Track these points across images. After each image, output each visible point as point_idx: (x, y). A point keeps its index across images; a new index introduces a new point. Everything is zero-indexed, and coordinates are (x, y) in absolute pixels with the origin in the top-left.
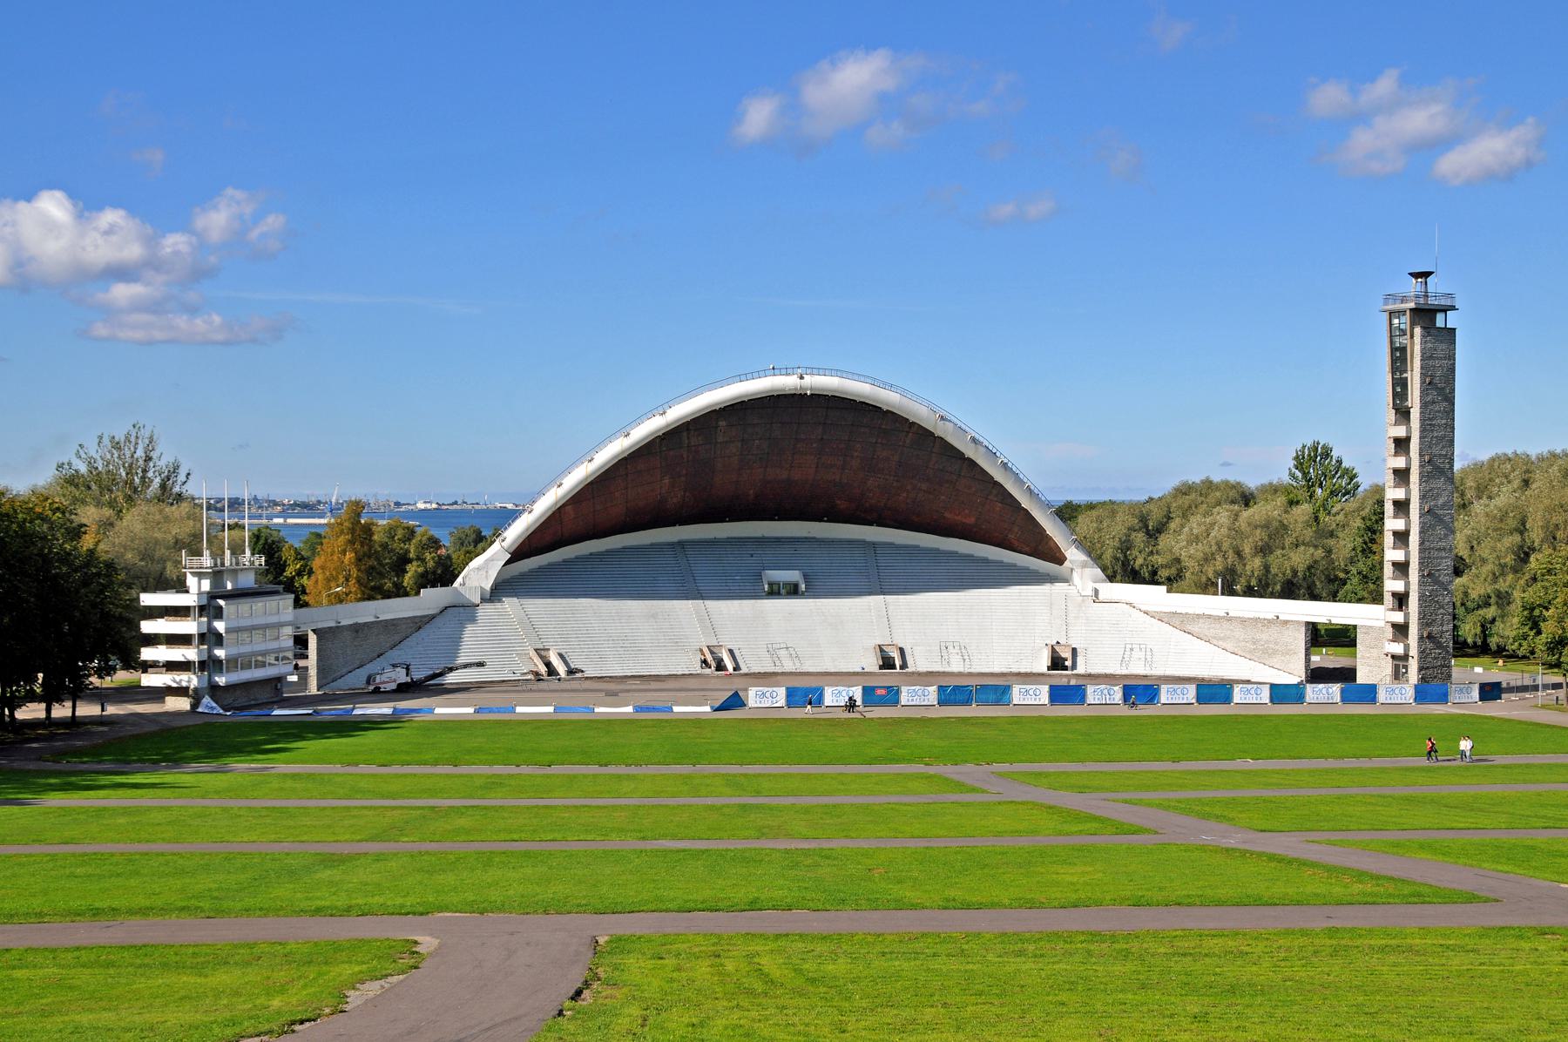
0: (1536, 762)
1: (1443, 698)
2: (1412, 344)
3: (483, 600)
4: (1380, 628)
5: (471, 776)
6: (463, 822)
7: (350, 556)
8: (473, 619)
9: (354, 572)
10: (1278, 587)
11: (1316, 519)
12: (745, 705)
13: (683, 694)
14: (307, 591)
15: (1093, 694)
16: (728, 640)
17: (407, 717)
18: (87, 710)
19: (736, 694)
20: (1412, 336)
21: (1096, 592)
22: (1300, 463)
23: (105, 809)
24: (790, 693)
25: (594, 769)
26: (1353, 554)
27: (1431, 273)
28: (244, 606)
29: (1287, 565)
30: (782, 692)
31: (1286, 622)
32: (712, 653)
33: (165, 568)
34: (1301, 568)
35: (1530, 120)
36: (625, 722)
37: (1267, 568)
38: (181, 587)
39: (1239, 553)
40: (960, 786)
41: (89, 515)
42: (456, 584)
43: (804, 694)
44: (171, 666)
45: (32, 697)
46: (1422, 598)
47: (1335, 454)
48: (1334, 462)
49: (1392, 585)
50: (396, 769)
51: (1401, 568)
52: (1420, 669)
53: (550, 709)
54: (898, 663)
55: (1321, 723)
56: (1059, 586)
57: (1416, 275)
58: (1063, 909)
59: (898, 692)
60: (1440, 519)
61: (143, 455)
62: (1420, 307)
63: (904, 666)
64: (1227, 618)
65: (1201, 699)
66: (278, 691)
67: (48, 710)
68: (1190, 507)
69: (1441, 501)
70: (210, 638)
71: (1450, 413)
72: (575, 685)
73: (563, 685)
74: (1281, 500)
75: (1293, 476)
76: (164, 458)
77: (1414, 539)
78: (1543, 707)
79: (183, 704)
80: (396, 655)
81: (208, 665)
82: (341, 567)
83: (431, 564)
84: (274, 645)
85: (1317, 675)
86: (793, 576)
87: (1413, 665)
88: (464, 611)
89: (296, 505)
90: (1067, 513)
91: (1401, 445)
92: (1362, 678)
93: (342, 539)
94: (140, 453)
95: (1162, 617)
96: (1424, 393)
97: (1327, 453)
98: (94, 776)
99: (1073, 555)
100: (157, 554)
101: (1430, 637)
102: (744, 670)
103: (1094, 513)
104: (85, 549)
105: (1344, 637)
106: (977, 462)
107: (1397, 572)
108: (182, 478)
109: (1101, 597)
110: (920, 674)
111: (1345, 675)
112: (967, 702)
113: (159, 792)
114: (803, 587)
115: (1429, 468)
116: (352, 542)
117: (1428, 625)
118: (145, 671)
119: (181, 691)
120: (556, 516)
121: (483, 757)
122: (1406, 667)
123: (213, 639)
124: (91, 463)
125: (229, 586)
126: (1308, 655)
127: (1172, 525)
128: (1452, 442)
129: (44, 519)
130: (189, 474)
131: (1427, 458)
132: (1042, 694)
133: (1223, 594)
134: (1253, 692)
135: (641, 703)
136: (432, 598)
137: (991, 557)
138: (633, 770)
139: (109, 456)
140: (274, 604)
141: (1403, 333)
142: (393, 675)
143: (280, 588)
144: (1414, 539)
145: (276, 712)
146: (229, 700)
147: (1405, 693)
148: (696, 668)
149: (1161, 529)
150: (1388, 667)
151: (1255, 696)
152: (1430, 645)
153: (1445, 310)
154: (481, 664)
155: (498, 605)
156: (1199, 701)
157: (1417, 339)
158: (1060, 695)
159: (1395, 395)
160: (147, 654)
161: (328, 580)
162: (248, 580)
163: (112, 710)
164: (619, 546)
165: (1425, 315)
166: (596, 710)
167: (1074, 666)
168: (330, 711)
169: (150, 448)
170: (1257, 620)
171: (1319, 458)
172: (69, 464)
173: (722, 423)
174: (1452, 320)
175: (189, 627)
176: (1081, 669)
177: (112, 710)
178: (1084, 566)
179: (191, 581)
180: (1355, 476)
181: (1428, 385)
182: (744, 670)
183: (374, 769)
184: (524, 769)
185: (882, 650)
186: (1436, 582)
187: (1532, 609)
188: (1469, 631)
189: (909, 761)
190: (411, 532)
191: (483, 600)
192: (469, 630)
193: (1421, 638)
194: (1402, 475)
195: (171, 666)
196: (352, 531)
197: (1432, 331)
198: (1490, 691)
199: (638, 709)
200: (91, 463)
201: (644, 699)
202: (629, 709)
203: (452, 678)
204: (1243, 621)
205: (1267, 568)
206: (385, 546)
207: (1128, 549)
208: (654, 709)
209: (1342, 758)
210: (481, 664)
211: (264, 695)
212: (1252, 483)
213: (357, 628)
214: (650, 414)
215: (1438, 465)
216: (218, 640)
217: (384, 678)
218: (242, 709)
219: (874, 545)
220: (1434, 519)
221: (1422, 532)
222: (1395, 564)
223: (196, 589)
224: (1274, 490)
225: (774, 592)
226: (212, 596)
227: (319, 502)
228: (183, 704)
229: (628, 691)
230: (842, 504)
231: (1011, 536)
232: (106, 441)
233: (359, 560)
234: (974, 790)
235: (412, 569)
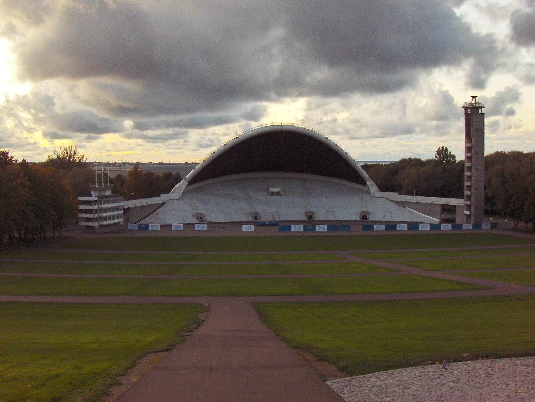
4: (463, 206)
15: (376, 227)
22: (439, 152)
48: (448, 153)
49: (467, 193)
61: (74, 152)
62: (473, 106)
65: (386, 228)
75: (436, 157)
94: (72, 152)
99: (370, 183)
105: (451, 209)
126: (441, 215)
130: (87, 158)
134: (446, 226)
139: (63, 153)
151: (202, 228)
153: (481, 108)
169: (76, 150)
171: (444, 151)
180: (455, 157)
213: (141, 207)
222: (467, 186)
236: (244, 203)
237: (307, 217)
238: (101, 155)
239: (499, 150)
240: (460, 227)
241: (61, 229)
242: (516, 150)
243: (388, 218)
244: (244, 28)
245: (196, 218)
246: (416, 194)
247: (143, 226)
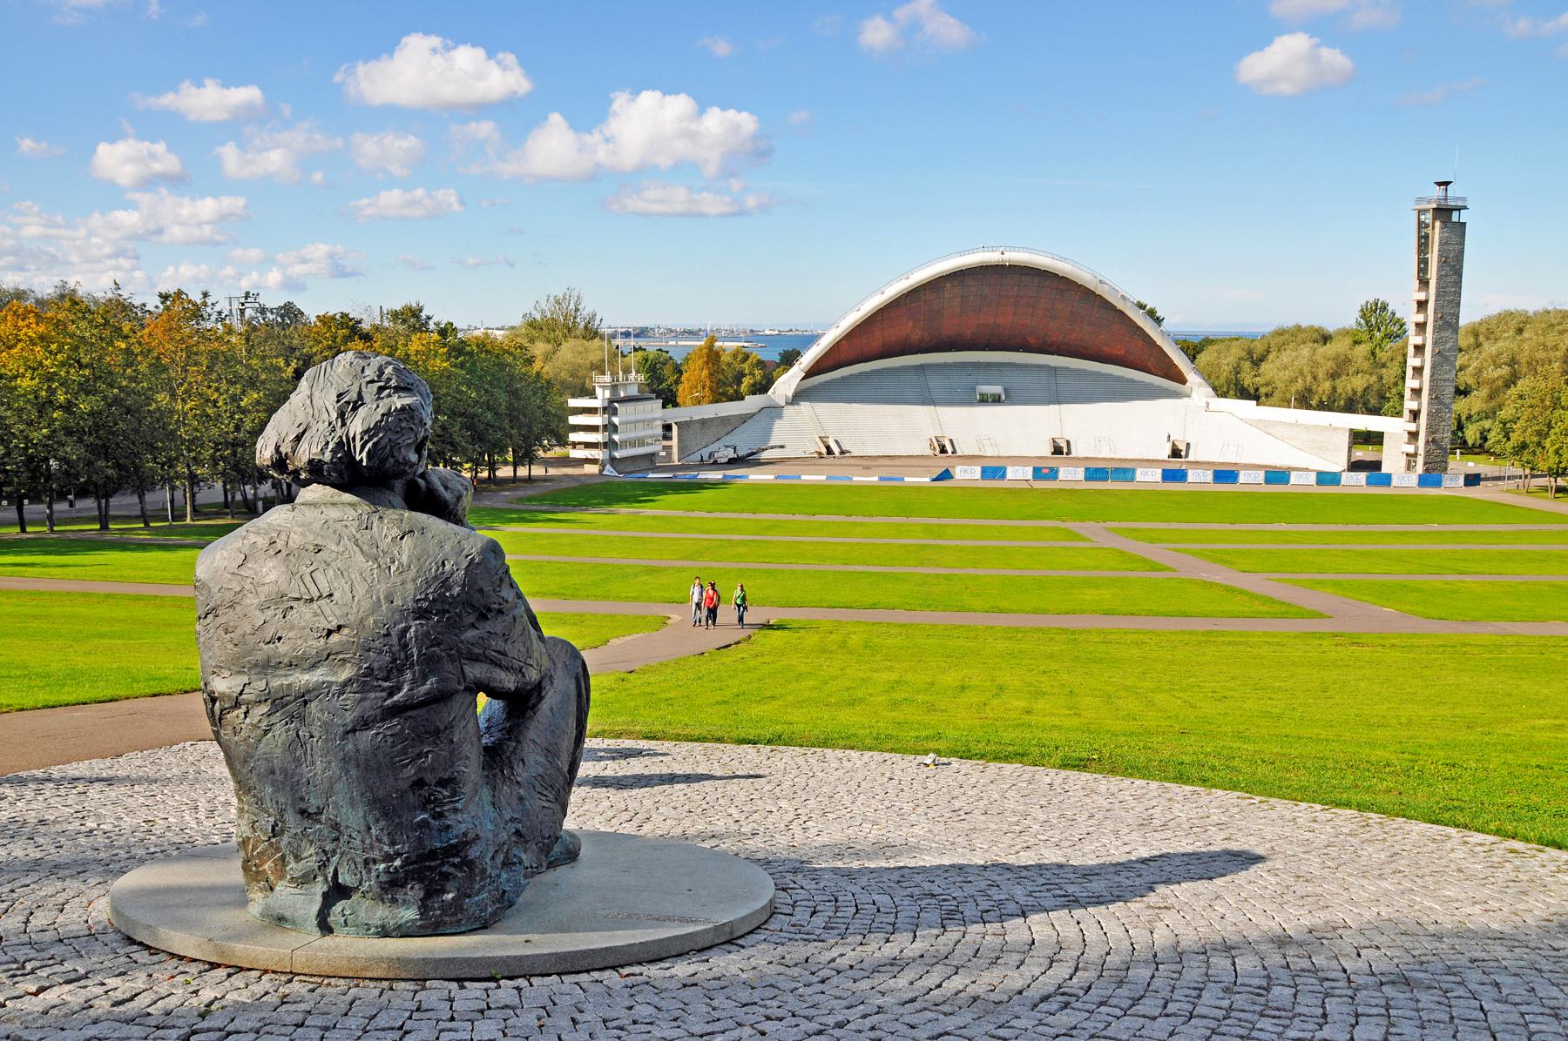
0: (1479, 529)
1: (1438, 484)
2: (1433, 234)
3: (787, 403)
5: (762, 520)
6: (742, 550)
7: (705, 372)
8: (780, 417)
9: (708, 384)
10: (1342, 403)
11: (1373, 354)
12: (952, 477)
13: (913, 469)
16: (948, 434)
17: (733, 481)
18: (538, 471)
19: (947, 470)
20: (1433, 228)
21: (1208, 404)
22: (1365, 313)
23: (538, 535)
24: (984, 470)
25: (842, 518)
27: (1450, 182)
28: (631, 407)
29: (1349, 387)
30: (978, 469)
31: (1336, 428)
32: (938, 441)
33: (585, 382)
34: (1360, 390)
36: (872, 488)
37: (1334, 389)
38: (591, 394)
39: (1315, 378)
40: (1075, 536)
41: (539, 348)
42: (769, 393)
43: (994, 471)
44: (588, 445)
45: (506, 463)
46: (1430, 414)
47: (1390, 308)
49: (1410, 404)
50: (717, 515)
51: (1417, 392)
52: (1425, 463)
53: (824, 478)
54: (1065, 450)
55: (1354, 501)
56: (1186, 399)
57: (1439, 184)
59: (1057, 472)
60: (1446, 359)
63: (1069, 453)
64: (1297, 424)
65: (1268, 481)
66: (652, 462)
67: (515, 471)
68: (1284, 344)
69: (1448, 346)
70: (610, 428)
71: (1458, 283)
72: (843, 461)
73: (837, 461)
74: (1348, 341)
76: (586, 312)
77: (1427, 372)
78: (1507, 491)
79: (593, 469)
80: (728, 440)
81: (609, 445)
82: (699, 380)
83: (758, 378)
84: (650, 432)
85: (1355, 466)
86: (997, 389)
87: (1420, 460)
88: (774, 411)
89: (685, 332)
90: (1193, 350)
91: (1422, 305)
92: (1384, 470)
93: (700, 362)
94: (572, 306)
95: (1252, 423)
96: (1440, 269)
97: (1384, 308)
98: (537, 514)
99: (1193, 378)
100: (580, 374)
101: (1433, 441)
102: (959, 453)
103: (1215, 347)
106: (1126, 312)
107: (1414, 396)
108: (597, 322)
109: (1211, 408)
110: (1079, 459)
111: (1375, 466)
112: (1105, 479)
113: (572, 525)
114: (1003, 397)
115: (1440, 323)
116: (707, 363)
117: (1433, 433)
118: (574, 448)
119: (594, 461)
120: (836, 347)
121: (772, 508)
122: (1415, 462)
123: (612, 428)
124: (543, 312)
125: (622, 395)
126: (1350, 451)
127: (1271, 357)
128: (1458, 304)
129: (510, 354)
131: (1439, 315)
132: (1156, 475)
133: (1295, 407)
135: (884, 475)
136: (752, 403)
137: (1136, 378)
138: (867, 519)
140: (633, 408)
141: (1427, 226)
142: (725, 453)
143: (654, 396)
144: (1427, 372)
145: (651, 475)
146: (621, 467)
147: (1413, 480)
148: (929, 452)
149: (1262, 359)
150: (1403, 461)
152: (1433, 447)
153: (1459, 209)
154: (782, 447)
155: (796, 407)
156: (1317, 484)
157: (1437, 230)
158: (1170, 476)
159: (1420, 270)
160: (573, 437)
161: (691, 388)
162: (633, 391)
163: (552, 471)
164: (880, 367)
165: (1443, 212)
166: (854, 479)
167: (1187, 456)
168: (684, 476)
170: (1316, 426)
172: (530, 314)
173: (948, 285)
174: (1464, 216)
175: (596, 420)
176: (1191, 458)
177: (552, 471)
179: (599, 391)
180: (1404, 324)
181: (1444, 262)
182: (959, 453)
183: (703, 514)
184: (798, 517)
185: (1054, 442)
186: (1441, 403)
187: (1505, 424)
188: (1471, 434)
189: (1051, 519)
190: (747, 357)
191: (787, 403)
192: (778, 424)
193: (1427, 442)
194: (1421, 327)
195: (588, 445)
196: (708, 356)
197: (1449, 225)
198: (1472, 480)
199: (881, 479)
200: (543, 312)
201: (885, 472)
202: (876, 479)
203: (765, 455)
204: (1307, 427)
205: (1334, 389)
206: (729, 364)
207: (1238, 373)
208: (892, 479)
209: (1347, 524)
210: (782, 447)
211: (645, 464)
212: (1331, 326)
213: (703, 422)
214: (898, 279)
215: (1448, 321)
216: (615, 429)
217: (720, 454)
218: (629, 473)
219: (1055, 369)
220: (1441, 358)
221: (1433, 368)
223: (602, 396)
224: (1345, 332)
225: (984, 400)
226: (611, 401)
227: (700, 330)
228: (593, 469)
229: (878, 466)
230: (1032, 341)
231: (1149, 364)
232: (551, 299)
233: (711, 374)
234: (1083, 539)
235: (746, 381)
240: (1386, 481)
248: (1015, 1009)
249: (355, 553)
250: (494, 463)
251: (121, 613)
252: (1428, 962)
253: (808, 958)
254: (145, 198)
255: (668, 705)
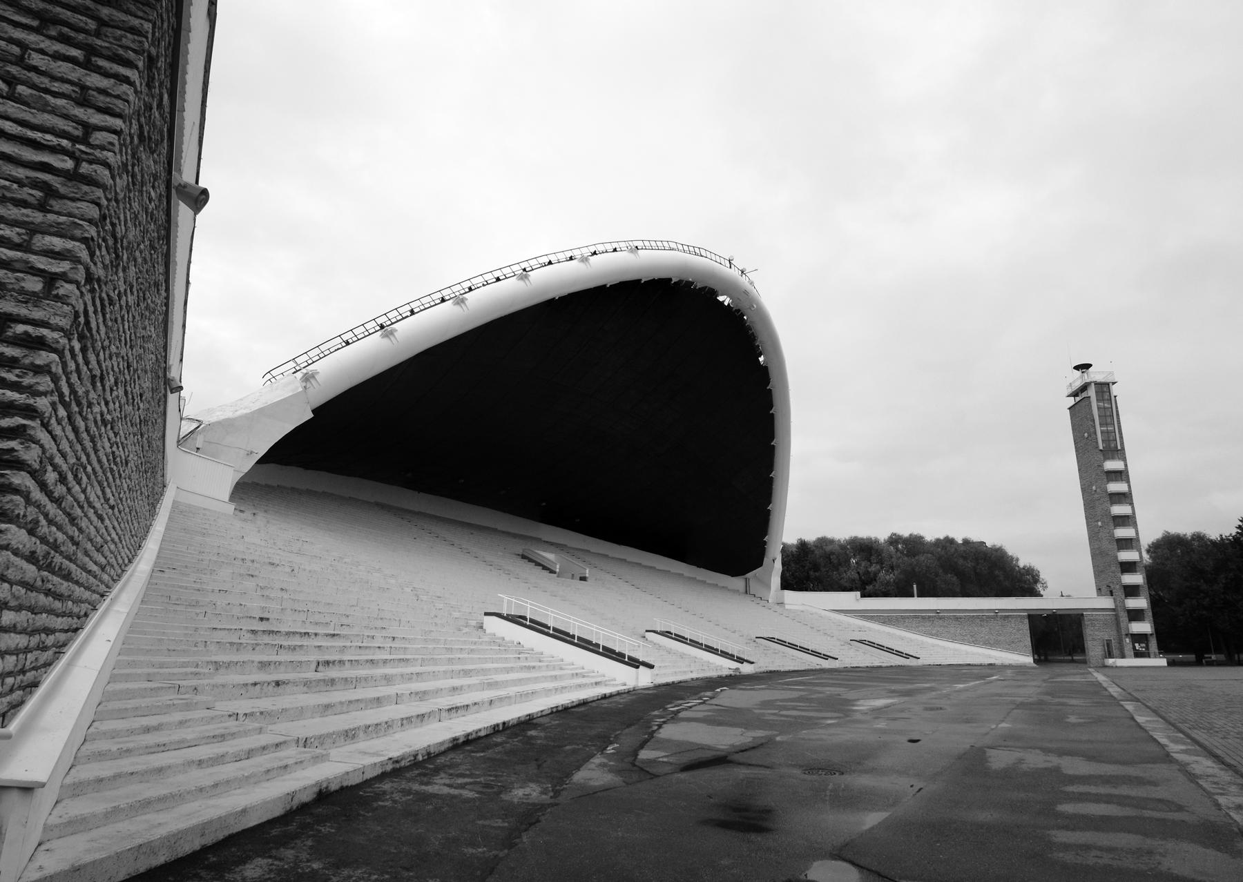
14: (1112, 519)
26: (177, 793)
35: (1150, 561)
58: (258, 700)
104: (1148, 560)
133: (919, 596)
178: (94, 114)
236: (982, 868)
237: (18, 711)
238: (519, 656)
239: (820, 537)
241: (10, 609)
242: (315, 793)
243: (500, 282)
244: (1011, 843)
245: (871, 592)
246: (119, 661)
247: (574, 772)
248: (394, 796)
249: (296, 698)
250: (17, 655)
251: (859, 674)
252: (140, 417)
253: (252, 452)
254: (418, 778)
255: (156, 422)
